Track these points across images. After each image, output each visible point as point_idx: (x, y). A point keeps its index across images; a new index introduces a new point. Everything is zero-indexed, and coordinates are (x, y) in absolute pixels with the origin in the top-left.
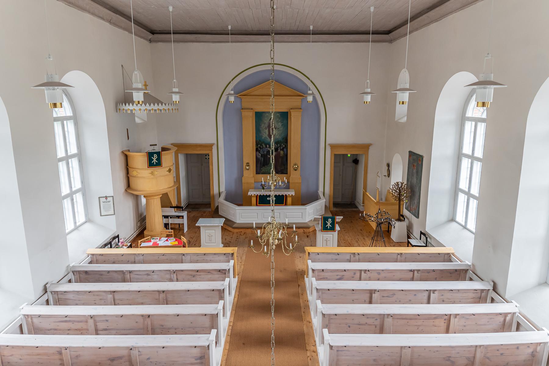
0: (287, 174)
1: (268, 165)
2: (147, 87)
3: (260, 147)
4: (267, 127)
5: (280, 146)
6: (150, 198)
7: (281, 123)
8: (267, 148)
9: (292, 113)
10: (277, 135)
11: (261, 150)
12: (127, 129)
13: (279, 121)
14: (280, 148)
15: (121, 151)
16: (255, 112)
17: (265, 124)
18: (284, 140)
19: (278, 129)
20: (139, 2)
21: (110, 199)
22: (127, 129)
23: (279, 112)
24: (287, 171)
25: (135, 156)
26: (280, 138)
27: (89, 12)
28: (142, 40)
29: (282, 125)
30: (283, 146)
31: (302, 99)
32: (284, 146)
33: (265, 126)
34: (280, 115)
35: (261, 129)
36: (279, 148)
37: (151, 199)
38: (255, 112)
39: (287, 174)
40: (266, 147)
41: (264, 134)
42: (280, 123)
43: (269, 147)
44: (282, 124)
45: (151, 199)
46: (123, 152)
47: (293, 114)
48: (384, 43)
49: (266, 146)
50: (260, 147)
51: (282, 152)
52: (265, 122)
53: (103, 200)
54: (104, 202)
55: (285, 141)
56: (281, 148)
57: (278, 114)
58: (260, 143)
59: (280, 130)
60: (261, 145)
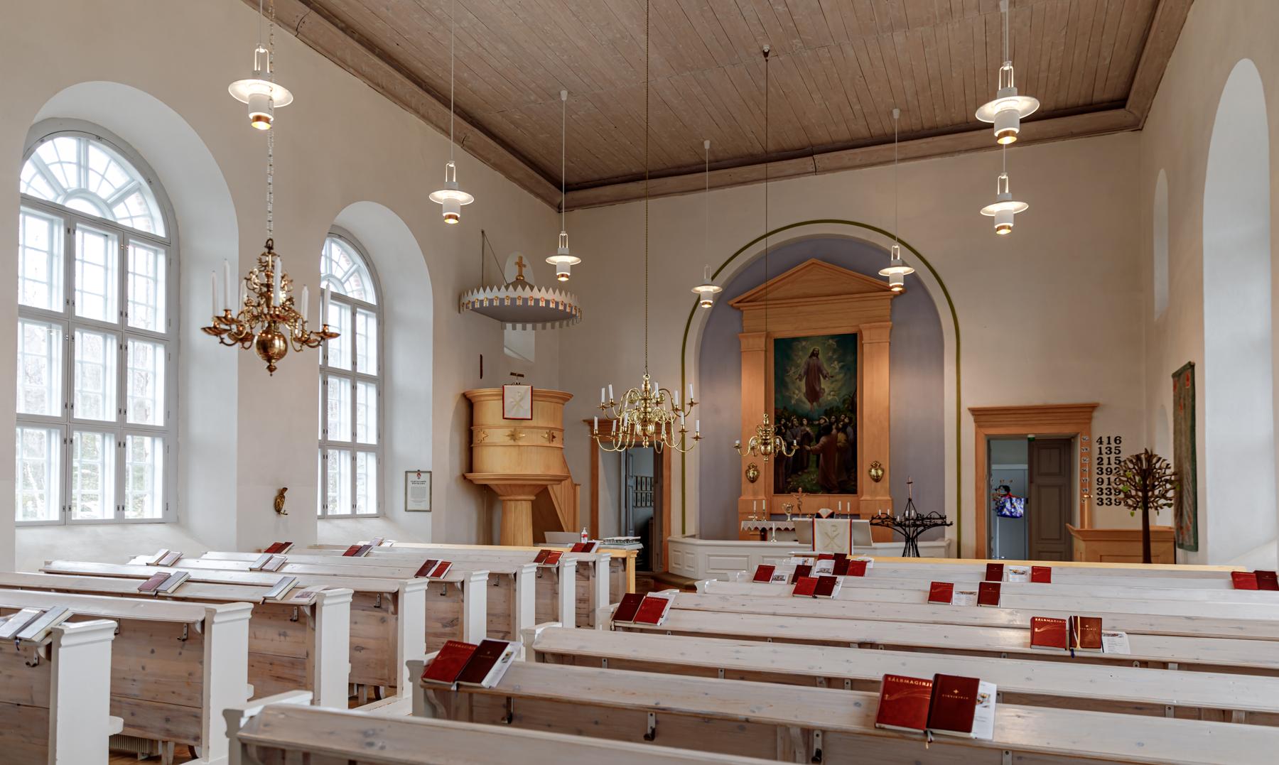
0: (855, 492)
1: (806, 471)
2: (523, 268)
3: (785, 425)
4: (802, 373)
5: (838, 420)
6: (508, 498)
7: (839, 362)
8: (803, 428)
9: (863, 333)
10: (829, 394)
11: (788, 432)
12: (481, 356)
13: (835, 357)
14: (837, 425)
15: (463, 392)
16: (775, 340)
17: (798, 366)
18: (846, 406)
19: (832, 377)
20: (504, 87)
21: (425, 477)
22: (481, 356)
23: (833, 337)
24: (856, 486)
25: (483, 399)
26: (836, 400)
27: (417, 112)
28: (539, 201)
29: (841, 368)
30: (843, 421)
31: (891, 299)
32: (847, 420)
33: (799, 373)
34: (836, 342)
35: (787, 379)
36: (834, 427)
37: (510, 500)
38: (775, 340)
39: (855, 492)
40: (802, 424)
41: (797, 392)
42: (836, 363)
43: (808, 423)
44: (842, 364)
45: (510, 500)
46: (464, 395)
47: (866, 335)
48: (1119, 135)
49: (802, 421)
50: (785, 425)
51: (841, 436)
52: (798, 362)
53: (413, 477)
54: (414, 482)
55: (850, 408)
56: (840, 426)
57: (831, 341)
58: (786, 415)
59: (836, 381)
60: (788, 419)
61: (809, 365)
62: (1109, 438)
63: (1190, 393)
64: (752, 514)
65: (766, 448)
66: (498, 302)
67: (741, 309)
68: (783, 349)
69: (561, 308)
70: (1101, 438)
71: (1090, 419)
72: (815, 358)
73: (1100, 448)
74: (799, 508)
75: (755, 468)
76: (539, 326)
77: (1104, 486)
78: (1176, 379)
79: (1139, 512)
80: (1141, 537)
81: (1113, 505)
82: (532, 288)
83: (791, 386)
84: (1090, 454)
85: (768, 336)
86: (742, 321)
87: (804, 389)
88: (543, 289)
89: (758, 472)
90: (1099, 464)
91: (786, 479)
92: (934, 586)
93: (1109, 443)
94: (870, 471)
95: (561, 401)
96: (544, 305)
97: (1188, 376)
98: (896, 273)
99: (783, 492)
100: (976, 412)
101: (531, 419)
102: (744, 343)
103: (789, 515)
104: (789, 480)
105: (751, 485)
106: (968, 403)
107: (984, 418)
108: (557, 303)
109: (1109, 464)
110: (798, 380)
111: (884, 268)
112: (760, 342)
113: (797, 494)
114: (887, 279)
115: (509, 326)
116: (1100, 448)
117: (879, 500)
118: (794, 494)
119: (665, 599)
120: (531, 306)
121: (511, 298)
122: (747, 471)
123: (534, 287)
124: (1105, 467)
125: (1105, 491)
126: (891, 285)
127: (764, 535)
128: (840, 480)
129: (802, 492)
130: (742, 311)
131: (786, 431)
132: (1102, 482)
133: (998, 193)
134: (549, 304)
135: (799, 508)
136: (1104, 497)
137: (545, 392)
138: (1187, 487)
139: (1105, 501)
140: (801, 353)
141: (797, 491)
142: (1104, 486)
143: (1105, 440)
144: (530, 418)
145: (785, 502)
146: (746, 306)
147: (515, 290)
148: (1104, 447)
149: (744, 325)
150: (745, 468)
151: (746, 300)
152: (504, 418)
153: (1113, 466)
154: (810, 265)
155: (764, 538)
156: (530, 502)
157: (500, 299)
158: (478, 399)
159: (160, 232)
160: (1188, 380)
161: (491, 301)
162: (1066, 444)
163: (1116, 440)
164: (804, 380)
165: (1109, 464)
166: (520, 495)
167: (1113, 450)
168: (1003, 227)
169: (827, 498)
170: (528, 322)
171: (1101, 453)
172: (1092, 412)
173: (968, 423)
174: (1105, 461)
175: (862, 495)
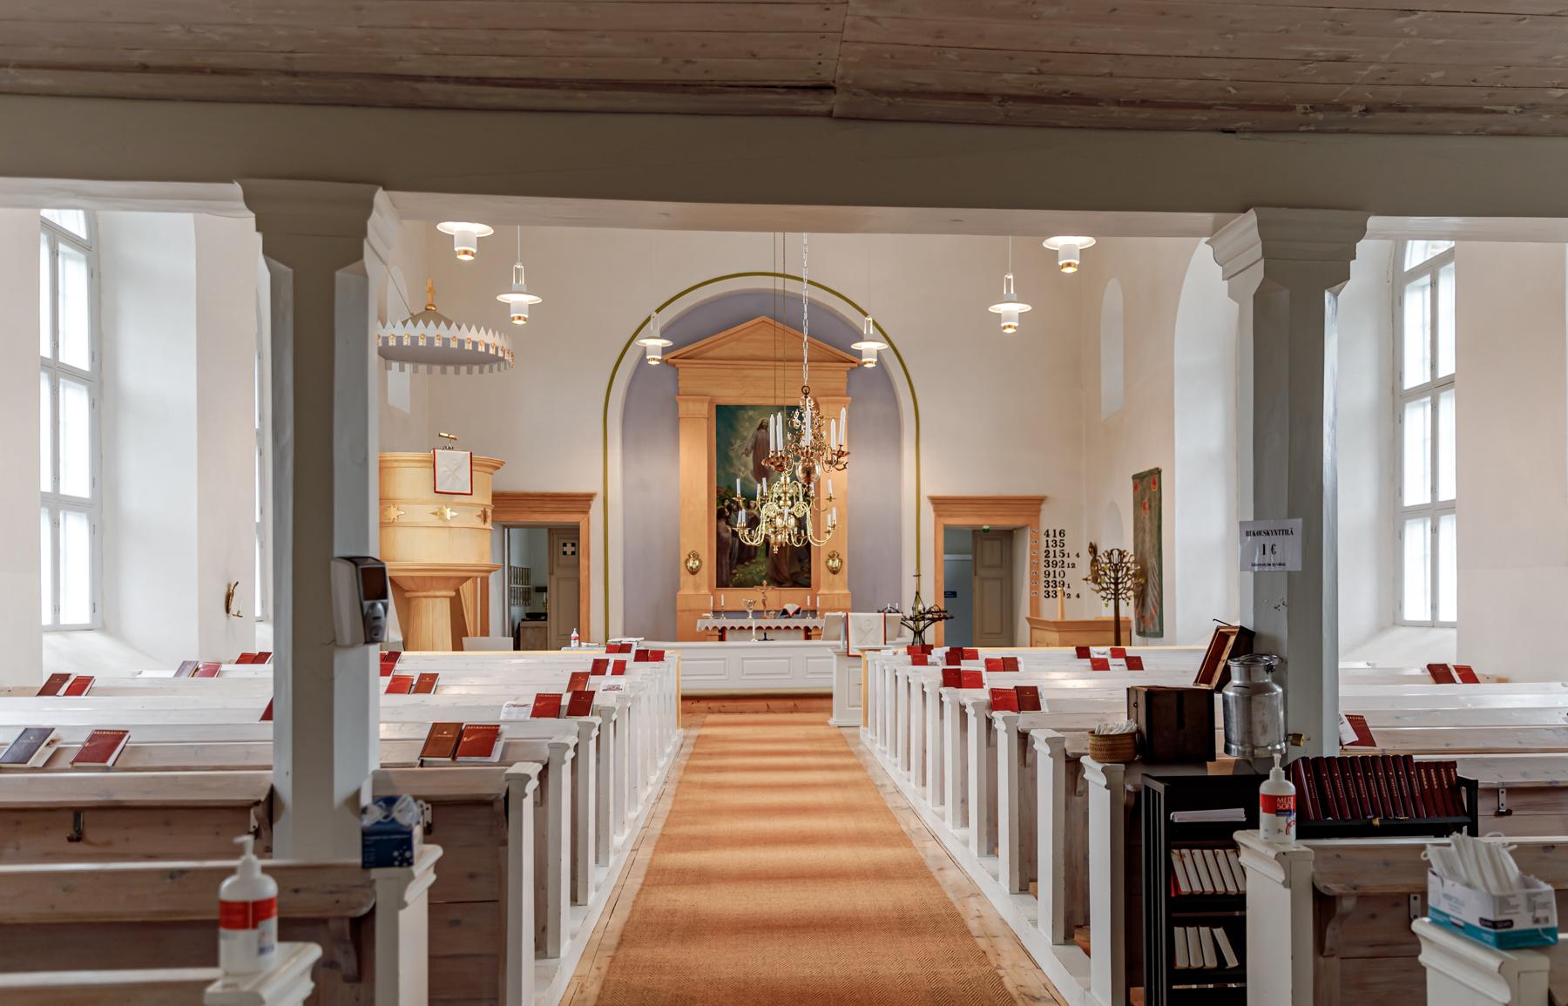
0: (809, 586)
1: (754, 561)
3: (729, 508)
4: (749, 448)
6: (425, 594)
16: (717, 406)
17: (744, 438)
31: (848, 372)
33: (745, 445)
35: (732, 454)
37: (426, 597)
38: (717, 406)
39: (809, 586)
41: (743, 469)
45: (426, 597)
50: (729, 508)
52: (745, 434)
61: (756, 438)
62: (1055, 531)
63: (1157, 496)
64: (707, 611)
65: (776, 536)
66: (425, 340)
67: (677, 366)
68: (727, 418)
69: (492, 351)
70: (1047, 531)
71: (1039, 511)
72: (764, 431)
73: (1047, 541)
74: (764, 604)
75: (696, 556)
76: (423, 368)
77: (1051, 579)
78: (1137, 481)
79: (1112, 603)
80: (1113, 627)
81: (1051, 597)
82: (449, 324)
83: (736, 462)
84: (1038, 548)
85: (711, 402)
86: (678, 381)
87: (751, 466)
88: (464, 327)
89: (700, 562)
90: (1046, 557)
91: (731, 570)
92: (540, 698)
93: (1055, 536)
94: (827, 562)
95: (490, 470)
96: (471, 348)
97: (1154, 480)
98: (870, 349)
99: (728, 586)
100: (936, 501)
101: (471, 494)
102: (683, 407)
103: (750, 612)
104: (734, 571)
105: (691, 577)
106: (929, 490)
107: (943, 507)
108: (487, 346)
109: (1055, 557)
110: (744, 456)
111: (856, 342)
112: (703, 409)
113: (761, 587)
114: (859, 354)
115: (395, 365)
116: (1047, 541)
117: (838, 594)
118: (758, 588)
119: (538, 716)
120: (468, 350)
121: (443, 339)
122: (687, 561)
123: (452, 323)
124: (1051, 559)
125: (1051, 584)
126: (864, 360)
127: (722, 634)
128: (793, 571)
129: (767, 585)
130: (678, 369)
131: (730, 514)
132: (1049, 575)
133: (1005, 293)
134: (477, 347)
135: (764, 604)
136: (1050, 589)
137: (482, 460)
138: (1152, 580)
139: (1051, 594)
140: (747, 424)
141: (761, 585)
142: (1051, 579)
143: (1051, 533)
144: (470, 492)
145: (733, 598)
146: (682, 363)
147: (437, 327)
148: (1050, 539)
149: (680, 385)
150: (683, 557)
151: (682, 356)
152: (436, 492)
153: (1058, 559)
154: (760, 323)
155: (722, 638)
156: (448, 600)
157: (397, 337)
158: (388, 465)
159: (83, 234)
160: (1154, 484)
161: (414, 339)
162: (1007, 537)
163: (1060, 533)
164: (751, 456)
165: (1055, 557)
166: (440, 589)
167: (1058, 543)
168: (1010, 326)
169: (778, 592)
170: (451, 363)
171: (1048, 546)
172: (1040, 504)
173: (928, 510)
174: (1052, 554)
175: (819, 589)
